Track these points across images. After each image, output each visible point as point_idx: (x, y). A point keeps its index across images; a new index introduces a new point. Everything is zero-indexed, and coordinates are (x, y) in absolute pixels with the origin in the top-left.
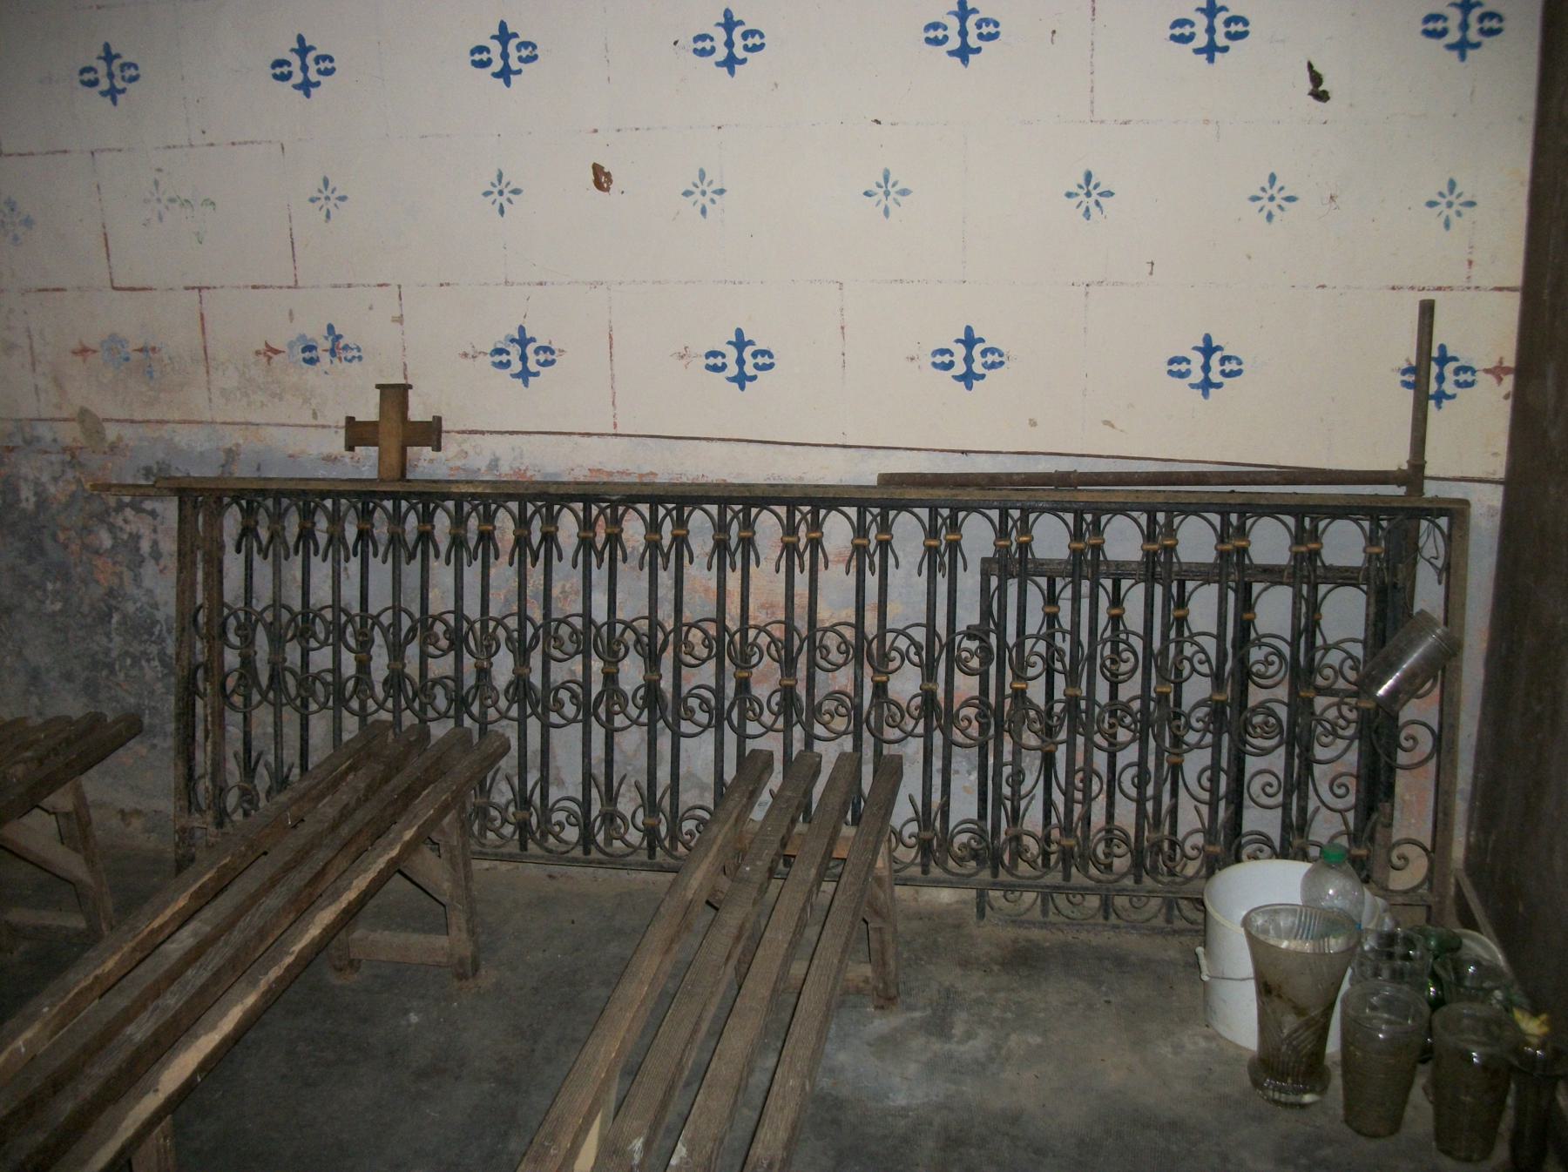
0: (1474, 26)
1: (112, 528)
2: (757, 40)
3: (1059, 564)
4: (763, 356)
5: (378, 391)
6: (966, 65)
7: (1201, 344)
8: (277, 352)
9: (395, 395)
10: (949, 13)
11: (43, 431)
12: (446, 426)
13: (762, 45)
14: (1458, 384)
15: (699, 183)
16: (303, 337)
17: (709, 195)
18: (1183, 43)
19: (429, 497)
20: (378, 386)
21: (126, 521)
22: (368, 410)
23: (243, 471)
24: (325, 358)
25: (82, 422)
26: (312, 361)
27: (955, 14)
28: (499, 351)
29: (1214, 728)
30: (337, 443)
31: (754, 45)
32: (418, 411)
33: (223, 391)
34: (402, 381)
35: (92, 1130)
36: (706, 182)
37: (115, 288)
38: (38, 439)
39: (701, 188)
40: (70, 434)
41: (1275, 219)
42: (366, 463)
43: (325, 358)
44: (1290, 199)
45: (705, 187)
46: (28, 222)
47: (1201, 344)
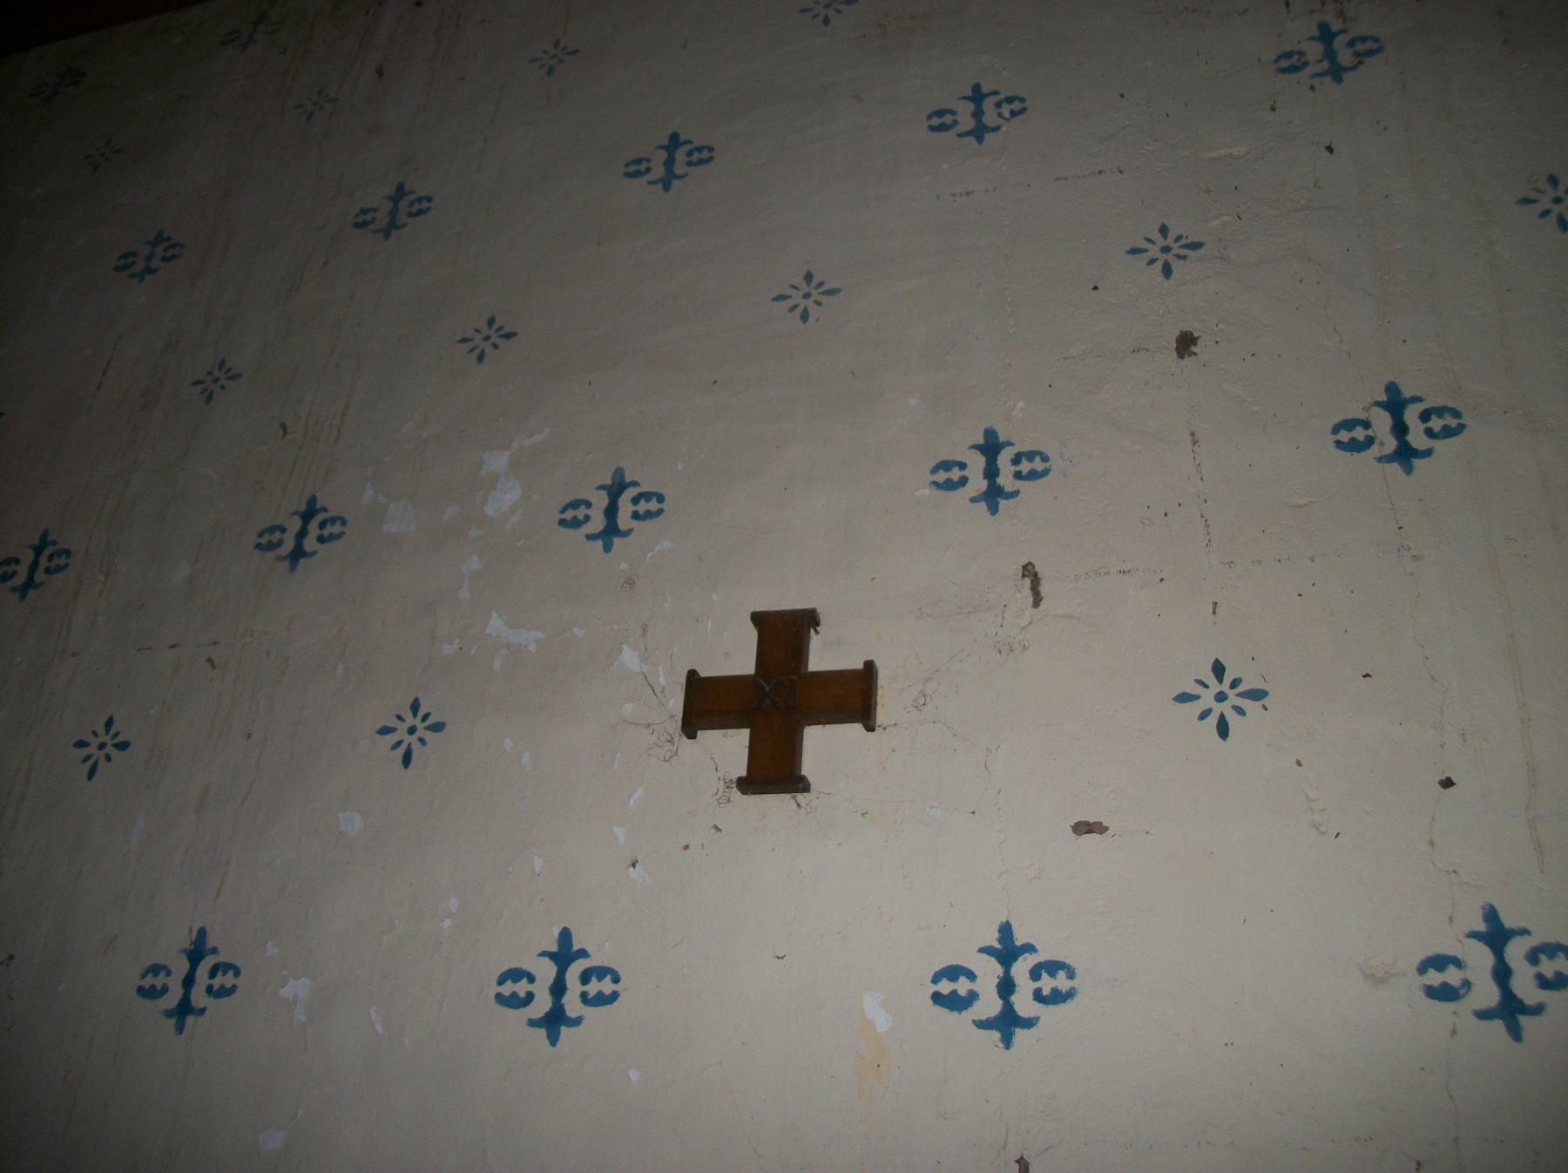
0: (1024, 988)
2: (607, 986)
4: (1551, 957)
5: (861, 666)
6: (1038, 1019)
7: (1481, 927)
10: (543, 954)
13: (615, 996)
15: (1241, 689)
17: (1218, 708)
18: (952, 1009)
20: (870, 667)
22: (823, 656)
27: (552, 956)
31: (600, 993)
32: (823, 656)
36: (1241, 702)
39: (1231, 694)
41: (811, 320)
45: (1233, 699)
47: (1481, 927)
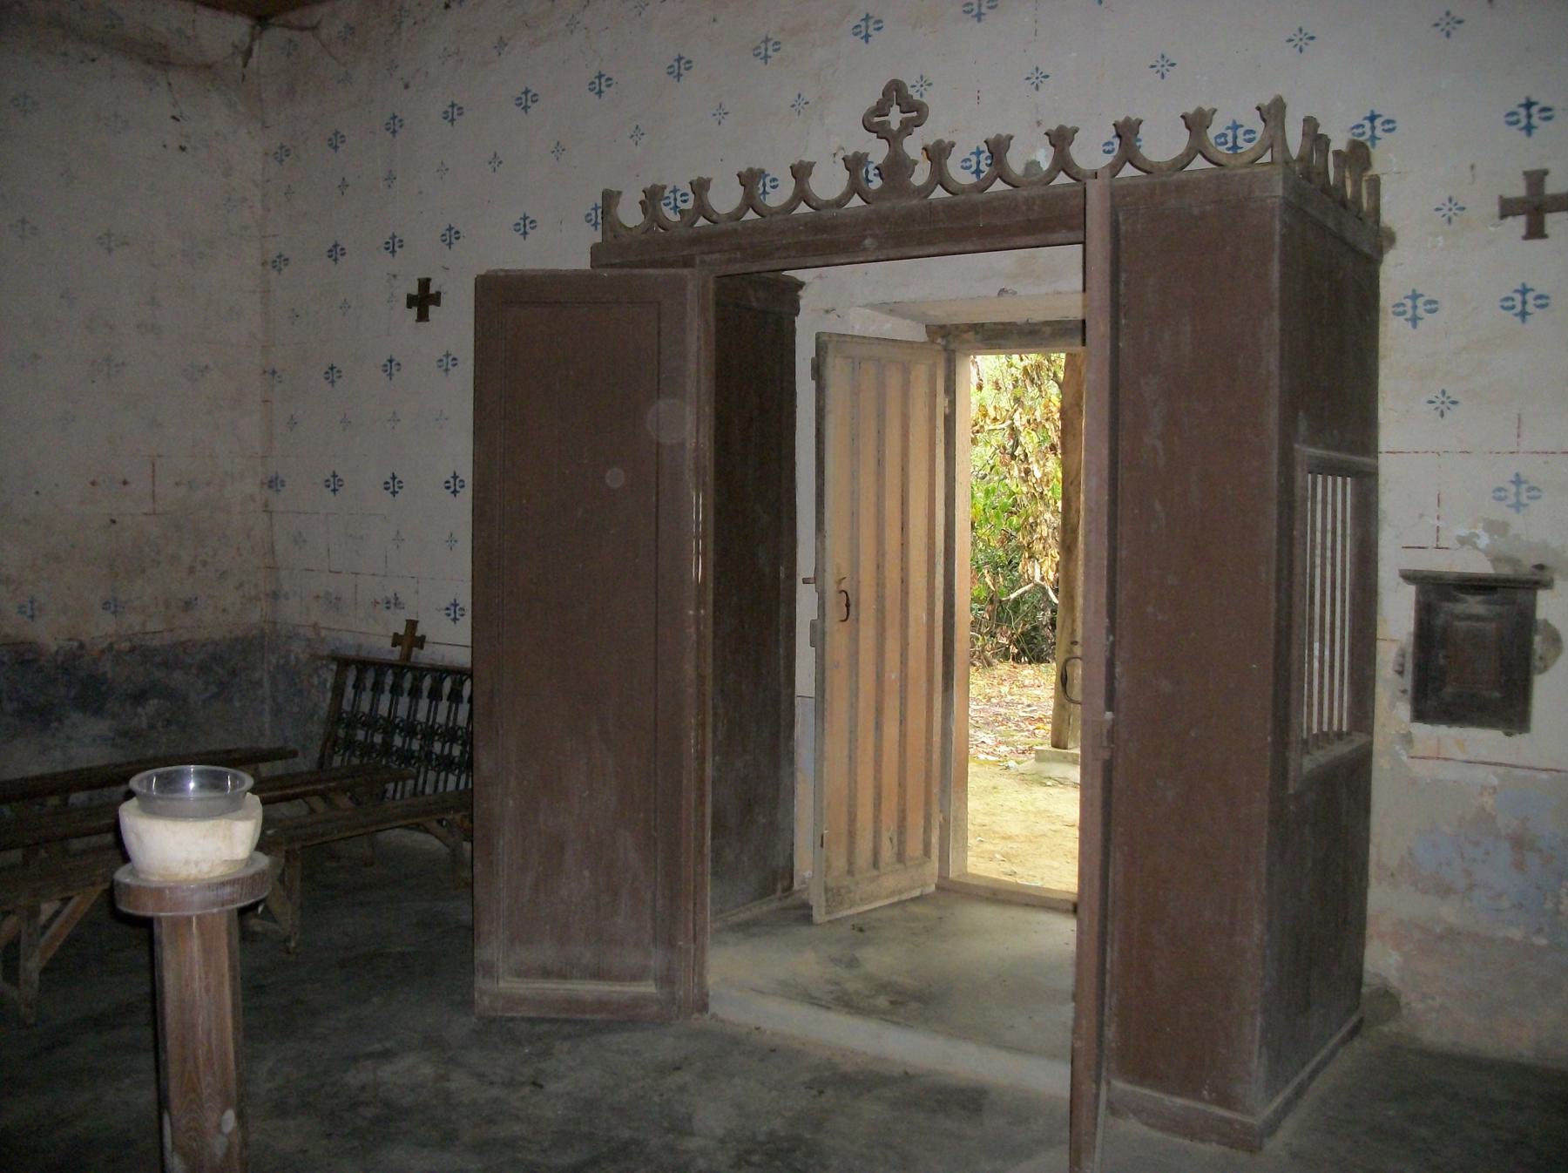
1: (319, 676)
3: (1041, 344)
8: (378, 603)
9: (412, 625)
11: (302, 631)
12: (427, 639)
14: (1403, 305)
16: (386, 597)
19: (420, 672)
21: (323, 673)
23: (363, 654)
24: (393, 607)
25: (314, 628)
26: (388, 608)
28: (448, 609)
29: (270, 837)
30: (388, 643)
33: (254, 501)
34: (415, 619)
35: (164, 961)
37: (330, 571)
38: (299, 634)
40: (310, 634)
42: (395, 654)
43: (393, 607)
44: (1163, 76)
46: (305, 541)
